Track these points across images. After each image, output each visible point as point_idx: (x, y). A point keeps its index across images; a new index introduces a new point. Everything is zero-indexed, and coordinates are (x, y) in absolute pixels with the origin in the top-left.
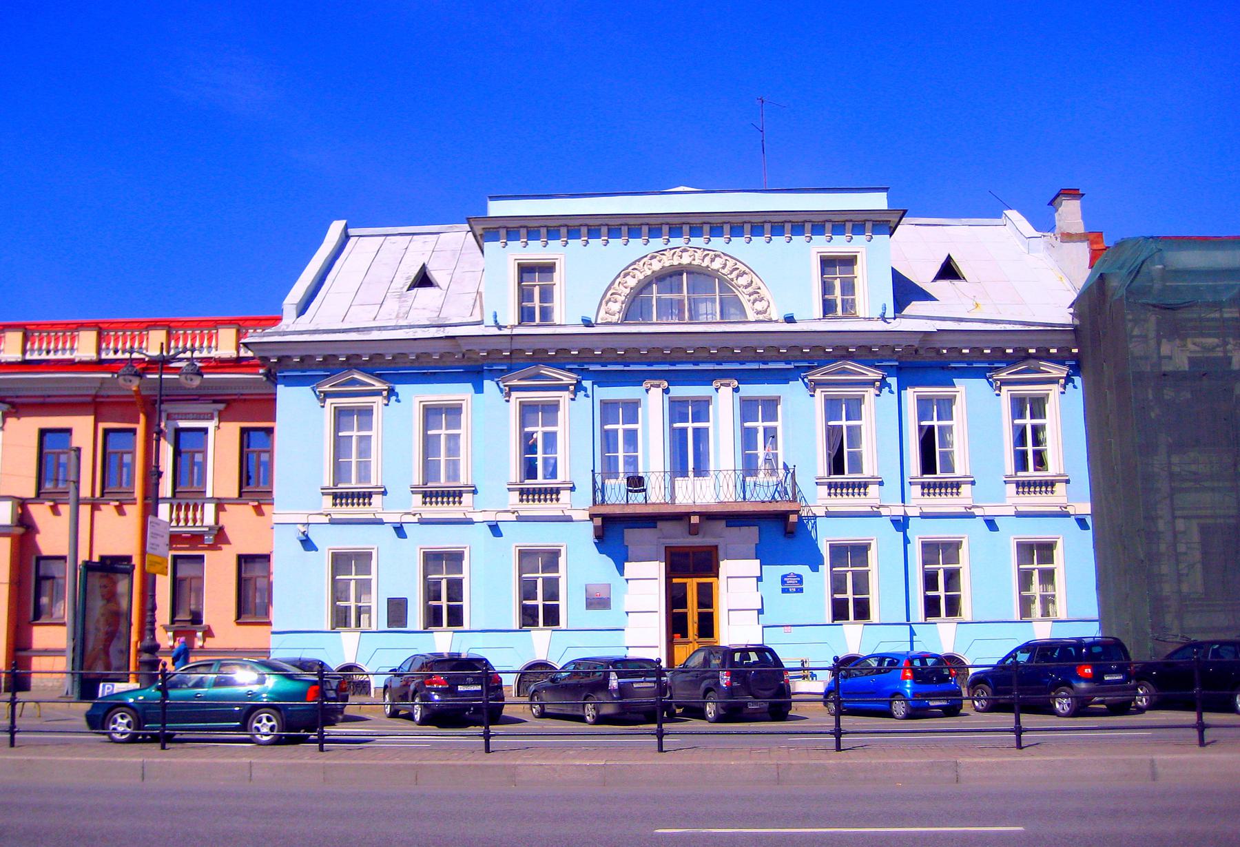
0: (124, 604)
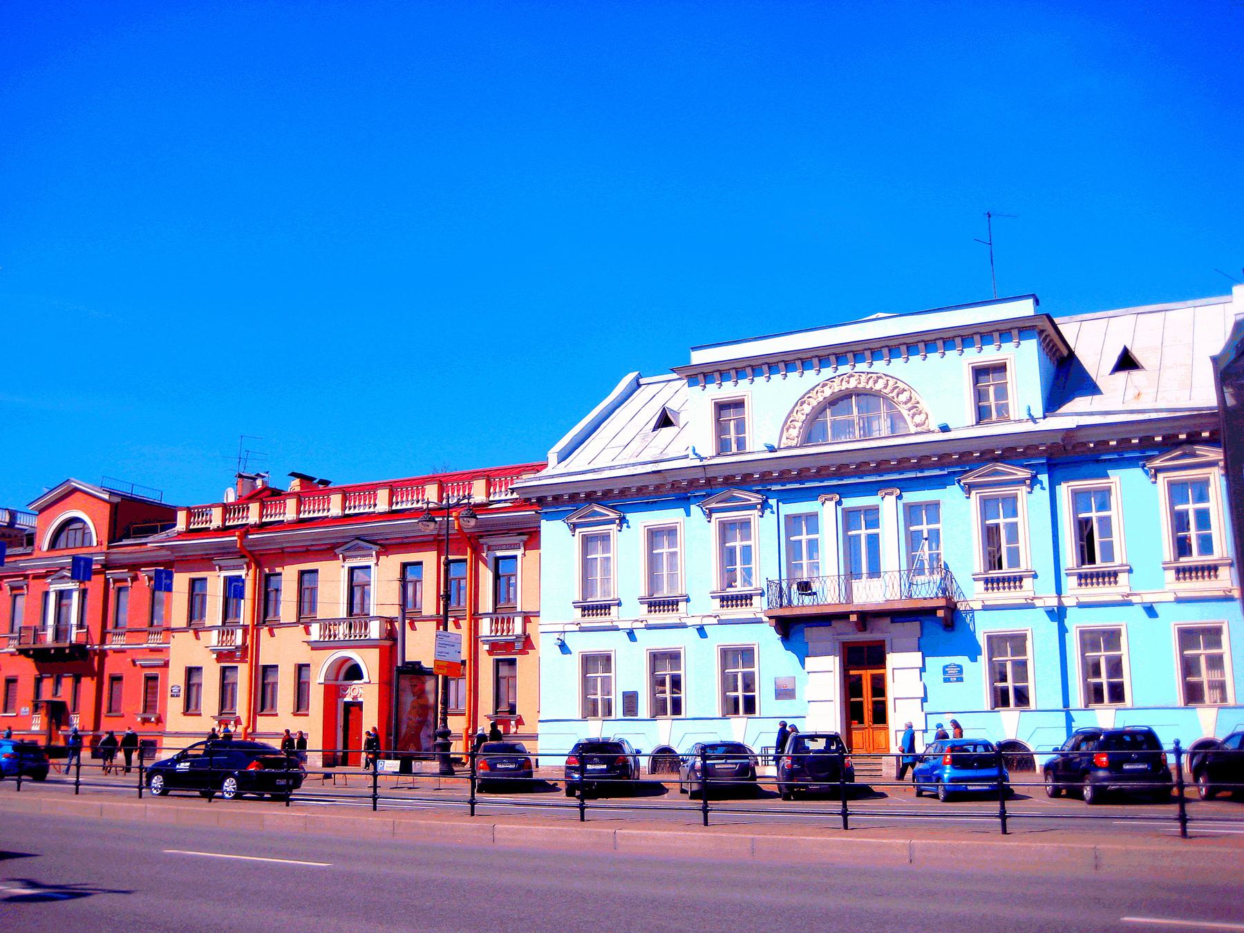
0: (431, 699)
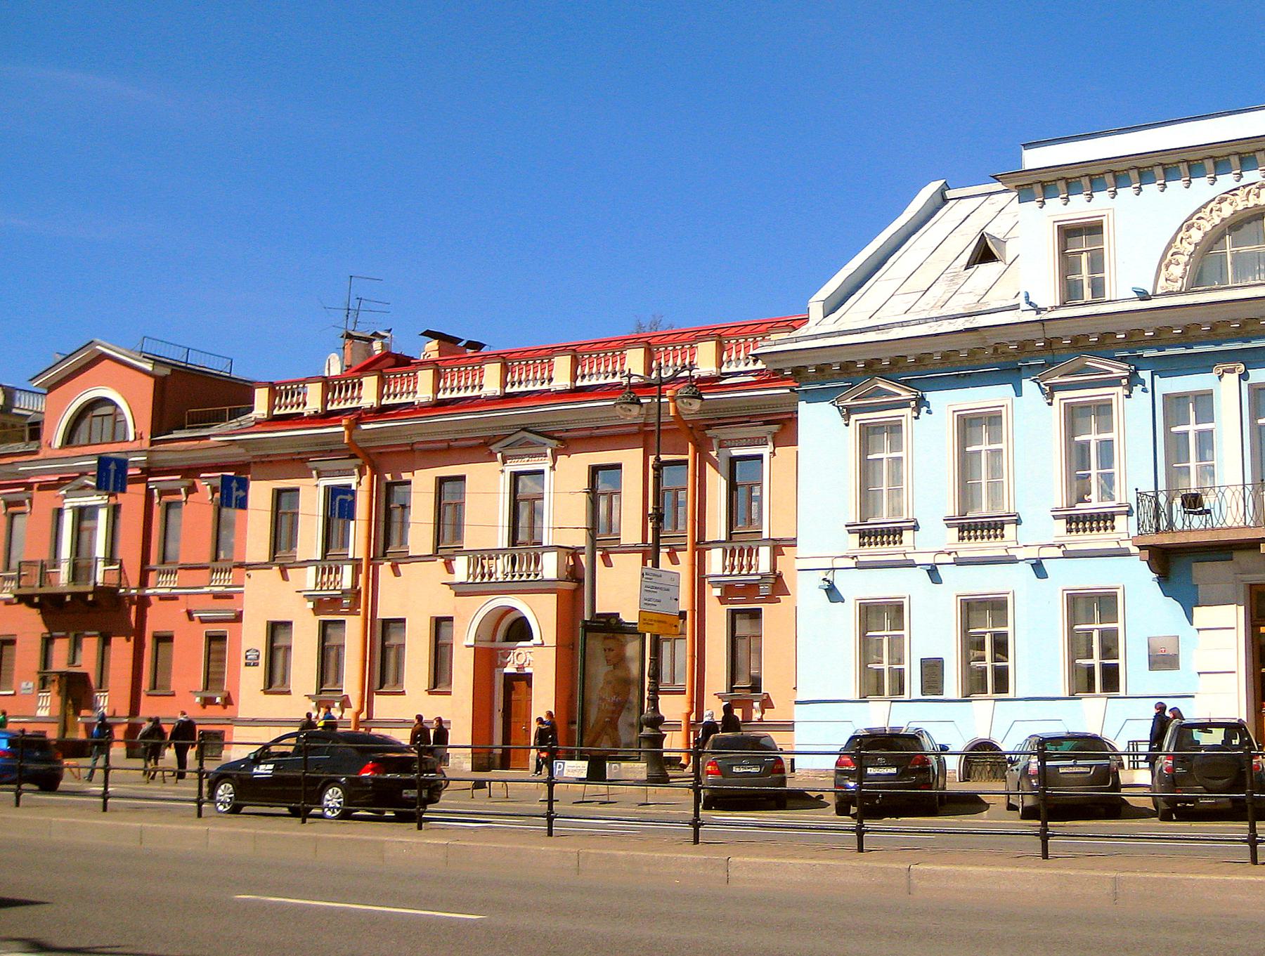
0: (634, 669)
